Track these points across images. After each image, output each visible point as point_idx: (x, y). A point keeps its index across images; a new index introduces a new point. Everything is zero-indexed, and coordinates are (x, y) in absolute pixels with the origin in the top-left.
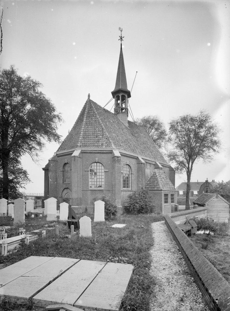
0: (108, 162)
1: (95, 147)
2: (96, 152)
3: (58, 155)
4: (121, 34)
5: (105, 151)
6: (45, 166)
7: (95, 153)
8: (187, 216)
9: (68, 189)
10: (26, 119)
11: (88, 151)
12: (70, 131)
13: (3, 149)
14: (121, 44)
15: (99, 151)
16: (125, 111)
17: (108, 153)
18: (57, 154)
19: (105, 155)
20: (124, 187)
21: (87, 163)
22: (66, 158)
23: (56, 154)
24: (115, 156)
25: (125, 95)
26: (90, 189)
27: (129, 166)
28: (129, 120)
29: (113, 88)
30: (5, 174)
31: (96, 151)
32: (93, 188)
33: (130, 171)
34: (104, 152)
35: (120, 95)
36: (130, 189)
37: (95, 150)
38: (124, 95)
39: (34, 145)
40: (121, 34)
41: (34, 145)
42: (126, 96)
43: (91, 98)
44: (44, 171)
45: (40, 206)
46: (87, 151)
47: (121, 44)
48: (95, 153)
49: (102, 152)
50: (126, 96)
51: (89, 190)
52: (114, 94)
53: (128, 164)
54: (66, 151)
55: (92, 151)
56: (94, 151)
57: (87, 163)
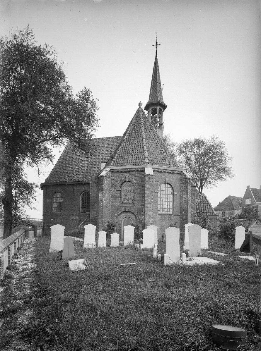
0: (177, 183)
1: (163, 165)
2: (166, 171)
3: (112, 171)
4: (157, 40)
5: (175, 171)
6: (45, 181)
7: (166, 172)
11: (159, 170)
14: (156, 51)
15: (169, 170)
17: (170, 173)
18: (111, 170)
19: (174, 175)
20: (84, 211)
21: (157, 183)
22: (127, 175)
23: (110, 170)
24: (188, 178)
25: (162, 109)
26: (159, 213)
30: (8, 191)
31: (167, 170)
32: (161, 212)
34: (174, 172)
37: (166, 168)
40: (157, 40)
45: (1, 238)
46: (158, 170)
47: (156, 51)
48: (166, 172)
49: (172, 172)
51: (159, 214)
54: (127, 167)
55: (162, 170)
56: (165, 171)
57: (157, 183)
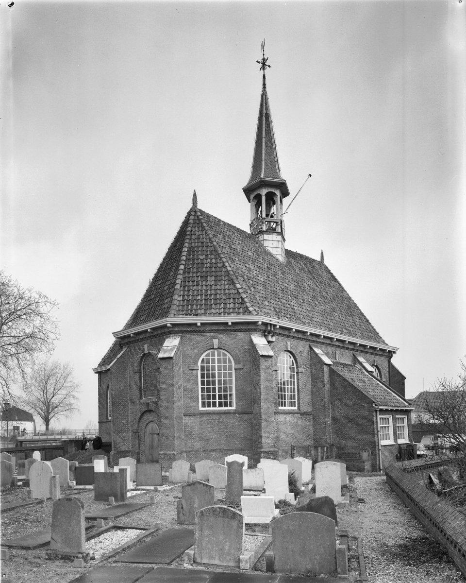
4: (264, 55)
8: (441, 468)
9: (152, 414)
10: (180, 274)
12: (151, 281)
13: (84, 438)
16: (277, 229)
25: (273, 191)
27: (289, 354)
28: (289, 249)
29: (245, 177)
33: (295, 367)
35: (264, 192)
36: (296, 408)
38: (257, 195)
39: (379, 487)
41: (379, 487)
42: (278, 193)
43: (199, 207)
44: (97, 375)
50: (278, 193)
52: (248, 191)
53: (289, 349)
